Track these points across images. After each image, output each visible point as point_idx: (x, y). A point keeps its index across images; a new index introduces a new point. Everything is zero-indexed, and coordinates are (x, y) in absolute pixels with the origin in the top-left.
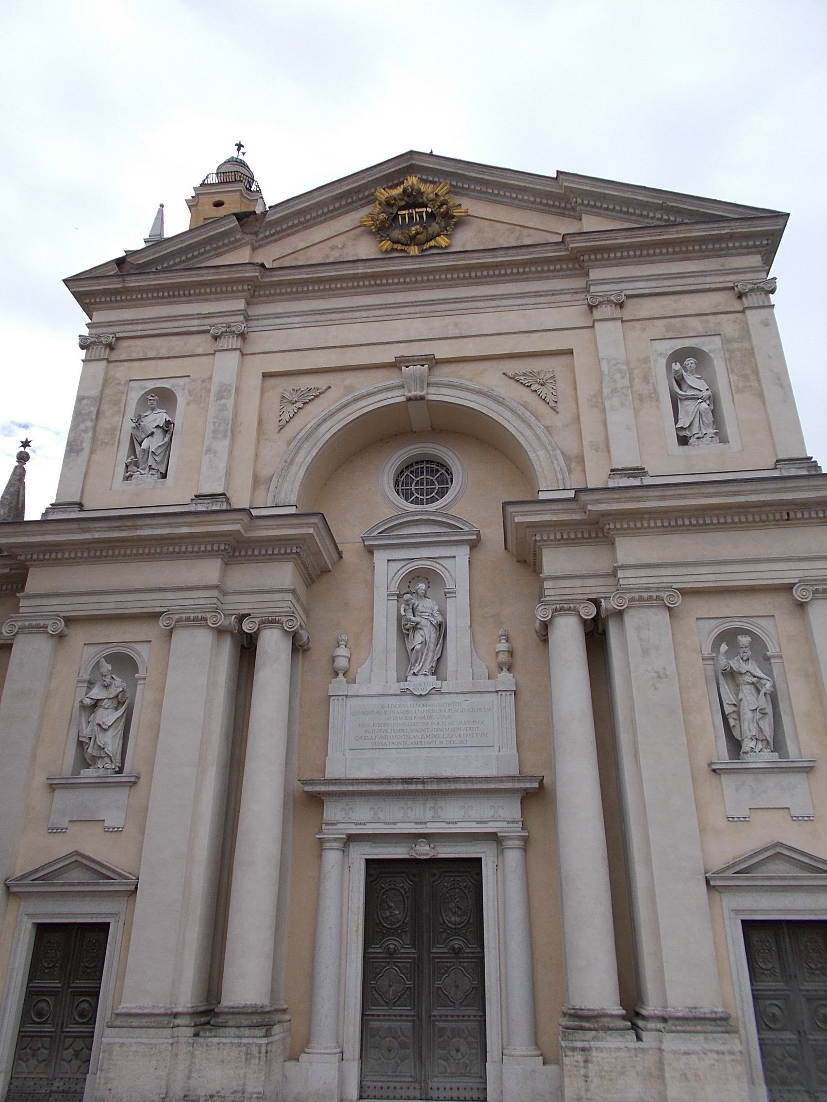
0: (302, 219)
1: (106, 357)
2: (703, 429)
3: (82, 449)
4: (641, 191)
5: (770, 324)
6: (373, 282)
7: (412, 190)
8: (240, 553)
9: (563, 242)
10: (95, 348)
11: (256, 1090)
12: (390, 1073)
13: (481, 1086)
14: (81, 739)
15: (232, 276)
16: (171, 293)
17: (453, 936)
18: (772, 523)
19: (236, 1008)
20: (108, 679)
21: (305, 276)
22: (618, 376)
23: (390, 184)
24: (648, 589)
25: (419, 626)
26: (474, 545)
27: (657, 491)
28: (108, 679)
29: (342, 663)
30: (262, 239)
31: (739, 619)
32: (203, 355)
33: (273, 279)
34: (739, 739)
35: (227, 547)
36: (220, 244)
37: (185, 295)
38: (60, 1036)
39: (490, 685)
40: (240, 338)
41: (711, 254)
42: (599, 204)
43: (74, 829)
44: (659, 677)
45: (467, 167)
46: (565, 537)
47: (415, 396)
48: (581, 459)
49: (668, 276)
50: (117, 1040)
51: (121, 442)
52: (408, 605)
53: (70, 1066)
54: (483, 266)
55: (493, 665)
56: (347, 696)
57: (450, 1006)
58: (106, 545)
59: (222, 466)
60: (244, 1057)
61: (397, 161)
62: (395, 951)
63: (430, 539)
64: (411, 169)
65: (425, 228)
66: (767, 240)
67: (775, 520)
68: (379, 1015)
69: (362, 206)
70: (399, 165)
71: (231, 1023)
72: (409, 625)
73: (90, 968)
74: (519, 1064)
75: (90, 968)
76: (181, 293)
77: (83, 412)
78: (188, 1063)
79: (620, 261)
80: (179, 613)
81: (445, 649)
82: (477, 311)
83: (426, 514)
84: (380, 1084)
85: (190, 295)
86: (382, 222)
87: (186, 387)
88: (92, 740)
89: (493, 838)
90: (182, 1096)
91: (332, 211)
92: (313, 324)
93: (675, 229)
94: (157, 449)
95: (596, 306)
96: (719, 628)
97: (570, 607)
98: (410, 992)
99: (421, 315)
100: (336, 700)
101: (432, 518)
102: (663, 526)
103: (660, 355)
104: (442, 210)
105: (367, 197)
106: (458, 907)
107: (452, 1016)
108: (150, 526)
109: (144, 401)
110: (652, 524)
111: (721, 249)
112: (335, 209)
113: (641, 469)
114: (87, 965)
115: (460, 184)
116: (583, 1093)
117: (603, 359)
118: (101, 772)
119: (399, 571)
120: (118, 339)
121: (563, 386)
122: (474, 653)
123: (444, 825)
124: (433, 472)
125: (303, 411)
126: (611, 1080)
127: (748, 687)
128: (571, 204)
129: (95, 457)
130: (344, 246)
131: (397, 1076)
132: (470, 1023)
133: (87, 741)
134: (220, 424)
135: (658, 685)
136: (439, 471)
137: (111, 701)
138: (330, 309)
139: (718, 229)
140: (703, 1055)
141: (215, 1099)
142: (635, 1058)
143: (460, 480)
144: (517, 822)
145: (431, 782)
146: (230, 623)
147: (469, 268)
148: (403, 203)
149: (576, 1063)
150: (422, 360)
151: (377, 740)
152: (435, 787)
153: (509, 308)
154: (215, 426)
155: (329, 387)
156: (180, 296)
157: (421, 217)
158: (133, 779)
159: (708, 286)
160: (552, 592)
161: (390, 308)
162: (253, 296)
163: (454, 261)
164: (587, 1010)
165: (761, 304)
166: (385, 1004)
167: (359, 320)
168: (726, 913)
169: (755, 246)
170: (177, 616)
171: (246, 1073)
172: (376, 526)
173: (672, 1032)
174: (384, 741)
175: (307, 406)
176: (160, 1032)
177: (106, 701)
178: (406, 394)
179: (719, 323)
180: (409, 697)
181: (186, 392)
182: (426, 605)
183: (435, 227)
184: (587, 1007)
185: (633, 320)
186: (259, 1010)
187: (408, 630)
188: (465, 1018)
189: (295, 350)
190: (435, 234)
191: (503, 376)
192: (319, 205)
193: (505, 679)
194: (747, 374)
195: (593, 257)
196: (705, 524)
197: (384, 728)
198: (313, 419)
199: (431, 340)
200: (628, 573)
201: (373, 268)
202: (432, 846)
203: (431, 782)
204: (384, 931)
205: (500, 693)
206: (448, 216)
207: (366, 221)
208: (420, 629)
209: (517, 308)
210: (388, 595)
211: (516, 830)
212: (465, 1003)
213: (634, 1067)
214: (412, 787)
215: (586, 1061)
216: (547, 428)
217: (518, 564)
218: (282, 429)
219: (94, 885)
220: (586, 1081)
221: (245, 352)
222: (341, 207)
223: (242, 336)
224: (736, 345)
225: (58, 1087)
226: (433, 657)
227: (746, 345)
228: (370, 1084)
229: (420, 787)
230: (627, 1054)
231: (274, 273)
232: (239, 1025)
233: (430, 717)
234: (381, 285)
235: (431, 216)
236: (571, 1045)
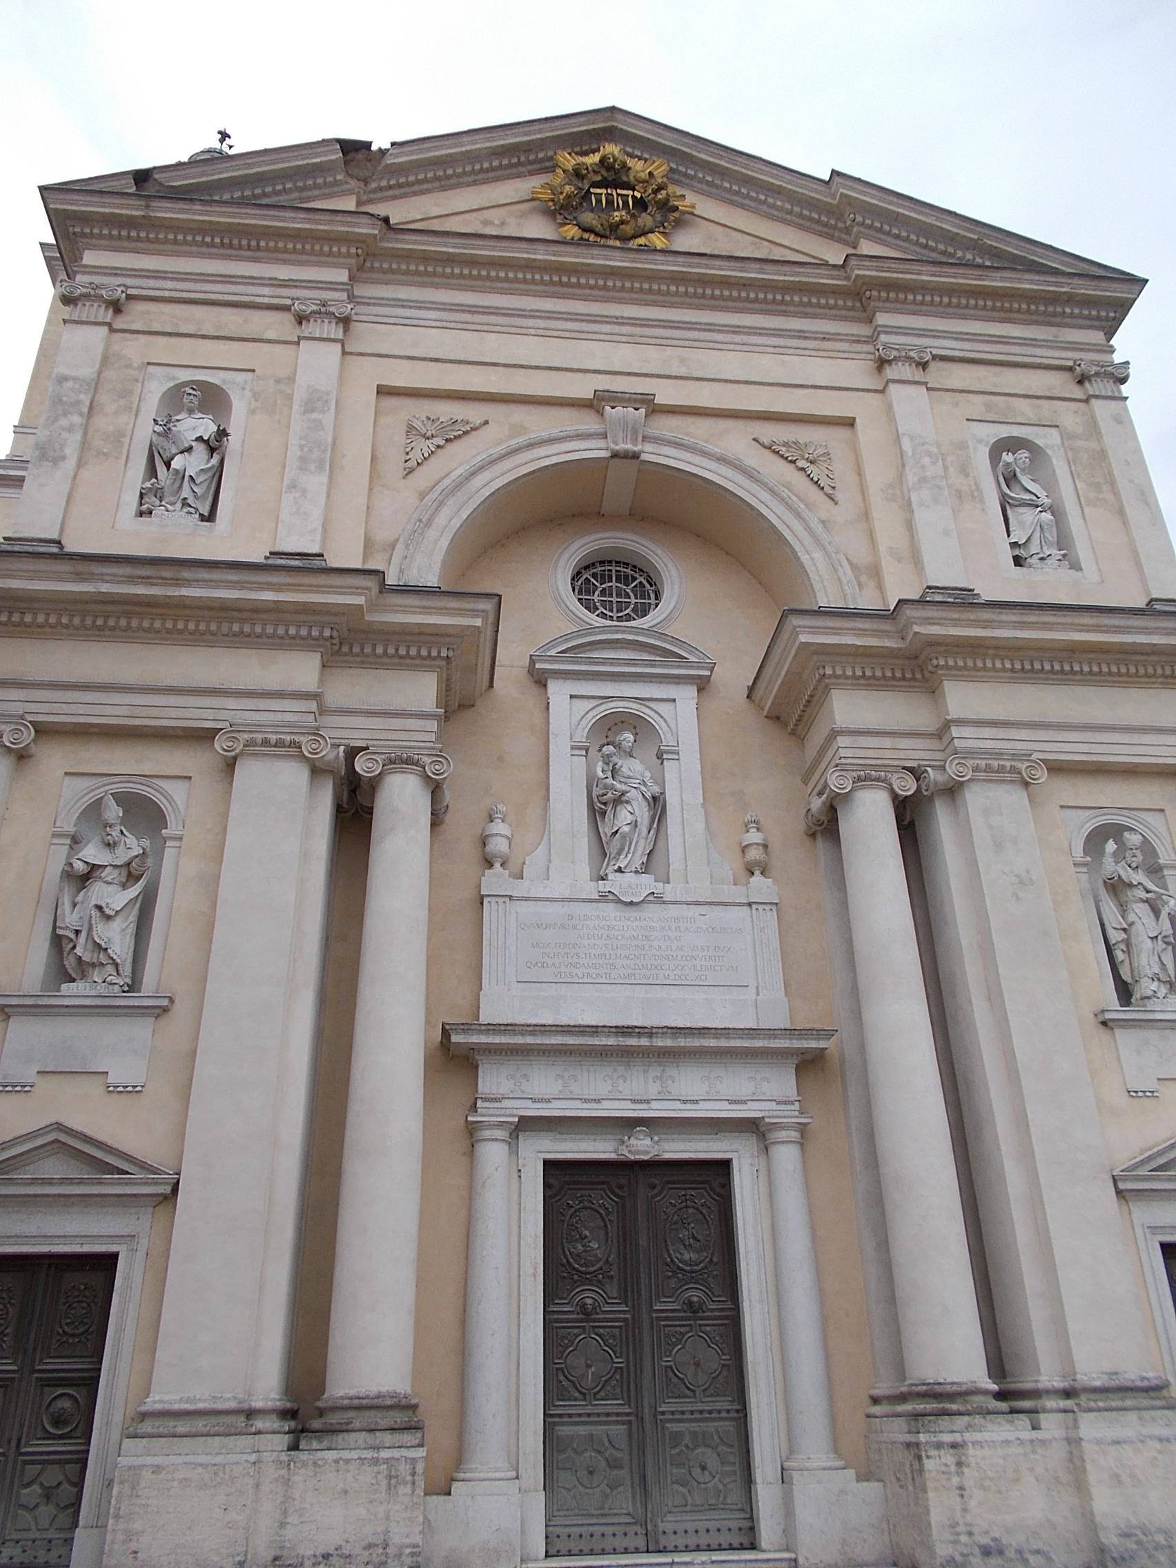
0: (440, 173)
1: (108, 320)
2: (1044, 548)
3: (64, 458)
4: (949, 218)
5: (1123, 420)
6: (556, 278)
7: (615, 160)
8: (351, 649)
9: (843, 266)
10: (87, 304)
11: (407, 1541)
12: (594, 1512)
13: (746, 1524)
14: (60, 932)
15: (335, 228)
16: (226, 241)
17: (687, 1284)
18: (1160, 680)
19: (363, 1398)
20: (115, 833)
21: (451, 250)
22: (926, 460)
23: (577, 149)
24: (999, 755)
25: (624, 798)
26: (702, 685)
27: (1014, 614)
28: (115, 833)
29: (498, 846)
30: (374, 191)
31: (1118, 811)
32: (278, 342)
33: (399, 246)
34: (1129, 980)
35: (335, 634)
36: (310, 182)
37: (249, 248)
38: (15, 1462)
39: (738, 894)
40: (341, 325)
41: (1041, 318)
42: (886, 228)
43: (46, 1086)
44: (1021, 882)
45: (696, 144)
46: (868, 673)
47: (626, 451)
48: (875, 572)
49: (986, 338)
50: (149, 1460)
51: (131, 456)
52: (608, 764)
53: (36, 1518)
54: (725, 282)
55: (738, 865)
56: (510, 897)
57: (686, 1397)
58: (120, 608)
59: (316, 513)
60: (384, 1482)
61: (589, 117)
62: (594, 1308)
63: (639, 670)
64: (609, 134)
65: (633, 216)
66: (1115, 312)
67: (1163, 676)
68: (570, 1416)
69: (531, 173)
70: (593, 123)
71: (357, 1424)
72: (610, 795)
73: (72, 1335)
74: (819, 1482)
75: (72, 1335)
76: (244, 242)
77: (65, 399)
78: (280, 1499)
79: (919, 308)
80: (250, 732)
81: (662, 833)
82: (711, 346)
83: (630, 633)
84: (577, 1530)
85: (258, 248)
86: (568, 196)
87: (248, 387)
88: (83, 935)
89: (754, 1128)
90: (270, 1558)
91: (487, 171)
92: (460, 326)
93: (998, 274)
94: (198, 474)
95: (889, 362)
96: (1092, 822)
97: (880, 776)
98: (622, 1375)
99: (630, 339)
100: (493, 903)
101: (640, 639)
102: (1013, 670)
103: (980, 441)
104: (660, 196)
105: (541, 161)
106: (694, 1238)
107: (692, 1412)
108: (207, 583)
109: (175, 399)
110: (998, 665)
111: (1055, 315)
112: (492, 169)
113: (970, 590)
114: (66, 1328)
115: (682, 169)
116: (958, 1514)
117: (904, 434)
118: (102, 989)
119: (593, 713)
120: (129, 297)
121: (842, 468)
122: (710, 845)
123: (678, 1105)
124: (627, 580)
125: (444, 451)
126: (1000, 1492)
127: (1141, 905)
128: (845, 222)
129: (85, 474)
130: (503, 224)
131: (604, 1515)
132: (721, 1423)
133: (72, 936)
134: (311, 450)
135: (1021, 895)
136: (636, 579)
137: (117, 872)
138: (488, 307)
139: (1056, 284)
140: (1139, 1444)
141: (334, 1560)
142: (1032, 1456)
143: (677, 591)
144: (792, 1103)
145: (663, 1033)
146: (337, 757)
147: (704, 281)
148: (599, 178)
149: (943, 1468)
150: (635, 401)
151: (563, 969)
152: (668, 1042)
153: (761, 349)
154: (302, 450)
155: (486, 422)
156: (240, 248)
157: (626, 203)
158: (165, 1002)
159: (1038, 360)
160: (849, 753)
161: (583, 321)
162: (361, 268)
163: (683, 266)
164: (949, 1384)
165: (1110, 394)
166: (580, 1397)
167: (532, 331)
168: (1139, 1231)
169: (1098, 318)
170: (246, 736)
171: (389, 1511)
172: (554, 642)
173: (1090, 1410)
174: (575, 971)
175: (450, 446)
176: (230, 1441)
177: (108, 868)
178: (612, 446)
179: (1055, 412)
180: (611, 905)
181: (247, 393)
182: (632, 767)
183: (646, 220)
184: (949, 1380)
185: (940, 390)
186: (404, 1402)
187: (605, 804)
188: (713, 1415)
189: (432, 360)
190: (646, 229)
191: (753, 442)
192: (469, 157)
193: (761, 886)
194: (1098, 483)
195: (884, 294)
196: (1072, 672)
197: (573, 951)
198: (461, 465)
199: (646, 375)
200: (967, 732)
201: (560, 256)
202: (656, 1138)
203: (663, 1033)
204: (576, 1277)
205: (754, 907)
206: (666, 207)
207: (541, 193)
208: (627, 802)
209: (772, 350)
210: (573, 748)
211: (790, 1114)
212: (711, 1391)
213: (1032, 1469)
214: (632, 1041)
215: (959, 1464)
216: (823, 522)
217: (766, 720)
218: (410, 473)
219: (93, 1184)
220: (962, 1496)
221: (347, 350)
222: (501, 167)
223: (345, 321)
224: (1080, 443)
225: (11, 1558)
226: (644, 851)
227: (1094, 445)
228: (558, 1530)
229: (644, 1041)
230: (1020, 1450)
231: (400, 237)
232: (373, 1427)
233: (647, 938)
234: (569, 285)
235: (641, 204)
236: (935, 1439)
